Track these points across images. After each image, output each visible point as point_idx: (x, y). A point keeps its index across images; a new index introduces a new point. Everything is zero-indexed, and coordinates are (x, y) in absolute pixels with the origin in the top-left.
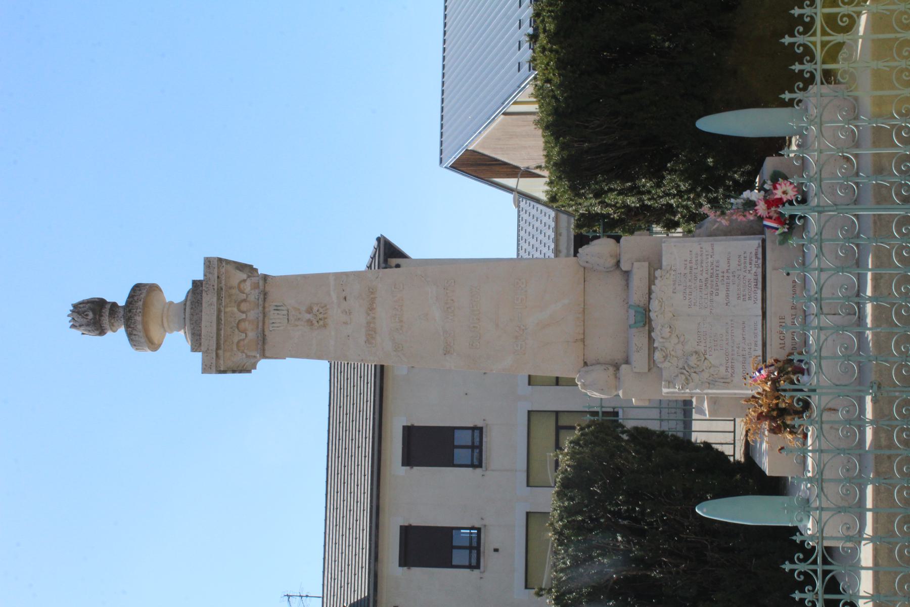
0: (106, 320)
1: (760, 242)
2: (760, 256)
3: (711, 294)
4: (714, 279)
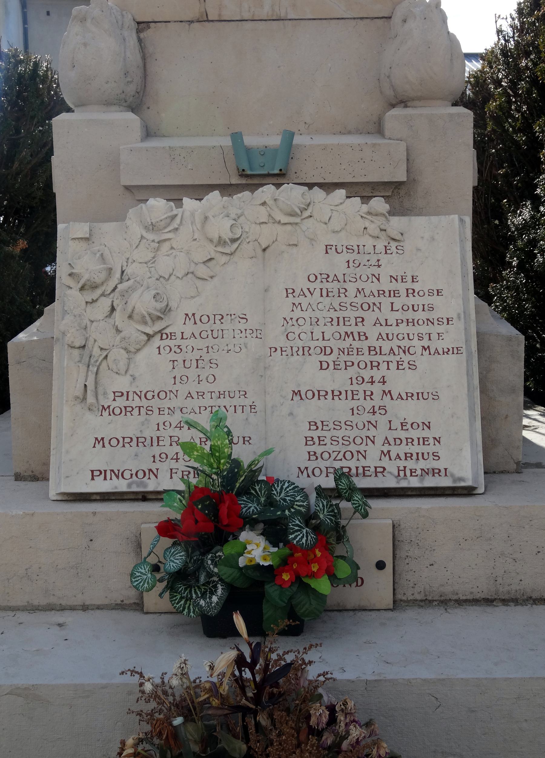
0: (350, 748)
1: (469, 483)
2: (430, 482)
3: (323, 350)
4: (367, 358)
